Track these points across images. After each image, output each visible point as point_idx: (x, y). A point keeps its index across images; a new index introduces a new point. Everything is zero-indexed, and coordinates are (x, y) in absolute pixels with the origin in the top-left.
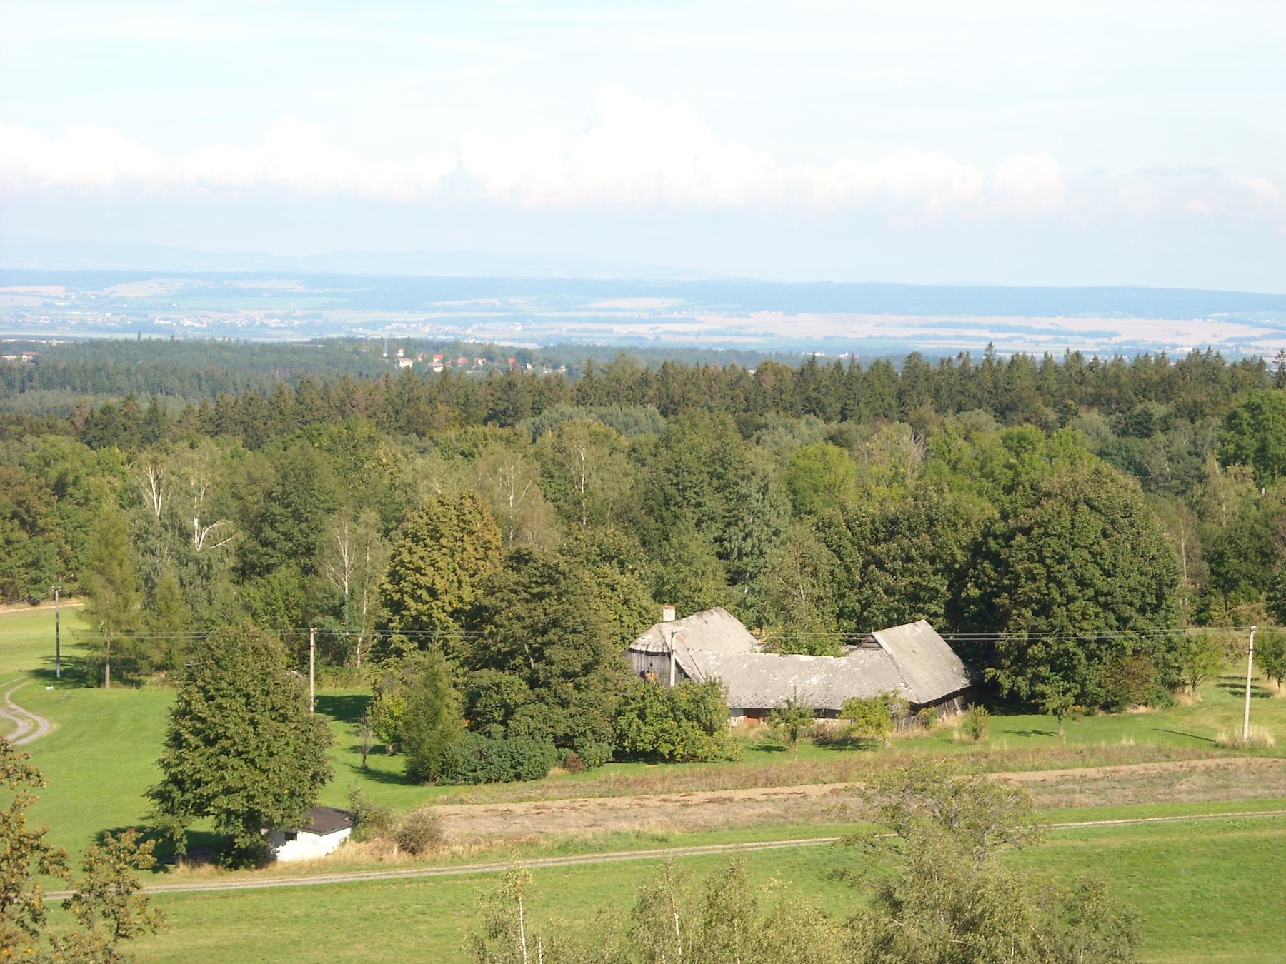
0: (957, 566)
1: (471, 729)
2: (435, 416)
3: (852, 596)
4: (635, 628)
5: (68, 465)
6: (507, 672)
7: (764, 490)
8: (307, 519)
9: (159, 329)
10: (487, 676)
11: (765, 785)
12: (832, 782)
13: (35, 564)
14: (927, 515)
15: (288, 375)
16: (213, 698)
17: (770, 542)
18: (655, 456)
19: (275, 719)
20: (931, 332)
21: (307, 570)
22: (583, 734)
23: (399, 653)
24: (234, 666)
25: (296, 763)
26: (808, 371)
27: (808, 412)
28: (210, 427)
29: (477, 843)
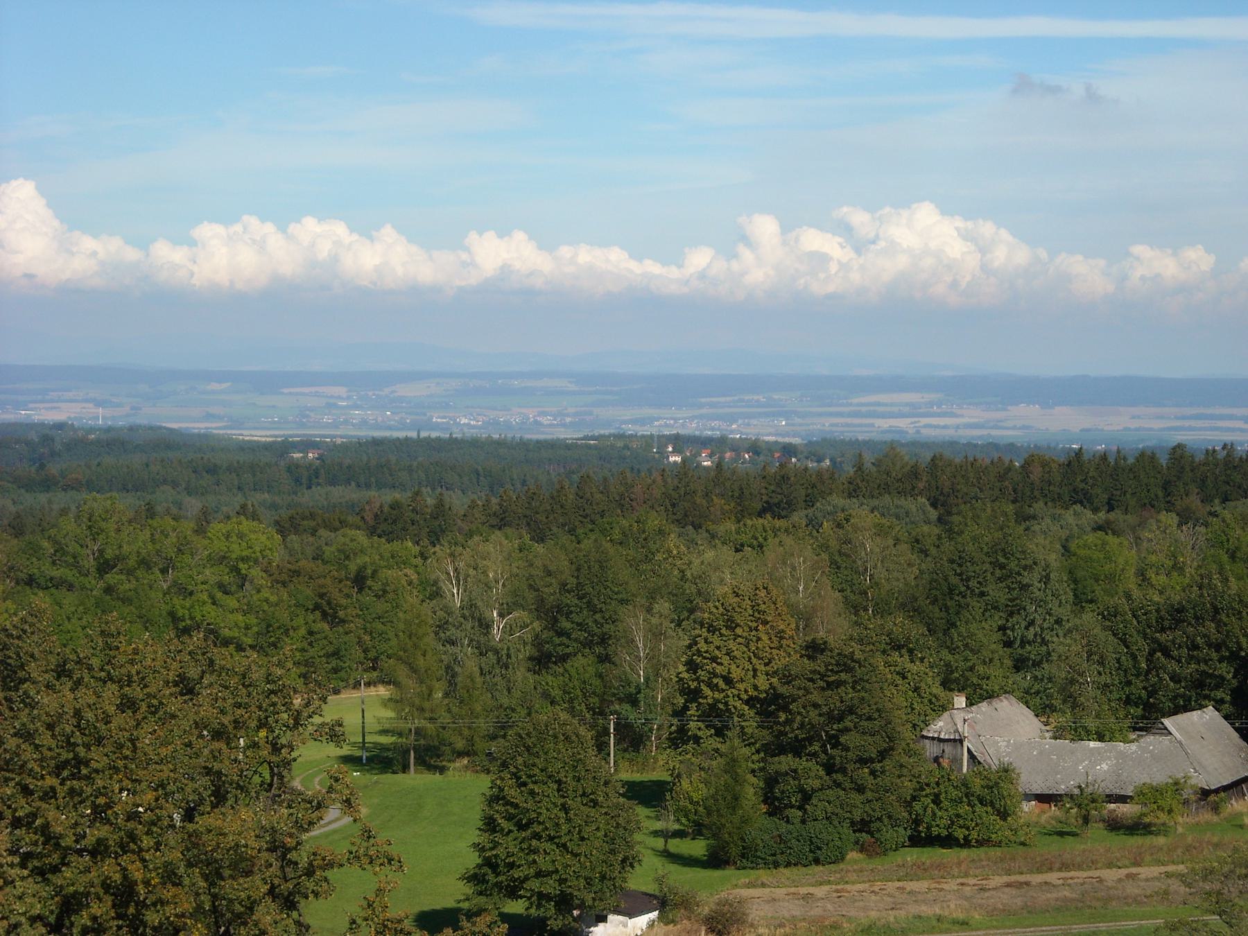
0: (1243, 654)
1: (770, 814)
2: (711, 509)
3: (1138, 683)
4: (926, 715)
5: (367, 559)
6: (804, 759)
7: (1046, 579)
8: (601, 611)
9: (437, 427)
10: (785, 762)
11: (1060, 870)
12: (1127, 867)
13: (336, 654)
14: (1212, 604)
15: (562, 470)
16: (525, 784)
17: (1052, 630)
18: (938, 546)
19: (586, 804)
20: (1187, 423)
21: (604, 659)
22: (880, 819)
23: (697, 739)
24: (546, 753)
25: (606, 847)
26: (1075, 462)
27: (1075, 503)
28: (494, 521)
29: (781, 925)
